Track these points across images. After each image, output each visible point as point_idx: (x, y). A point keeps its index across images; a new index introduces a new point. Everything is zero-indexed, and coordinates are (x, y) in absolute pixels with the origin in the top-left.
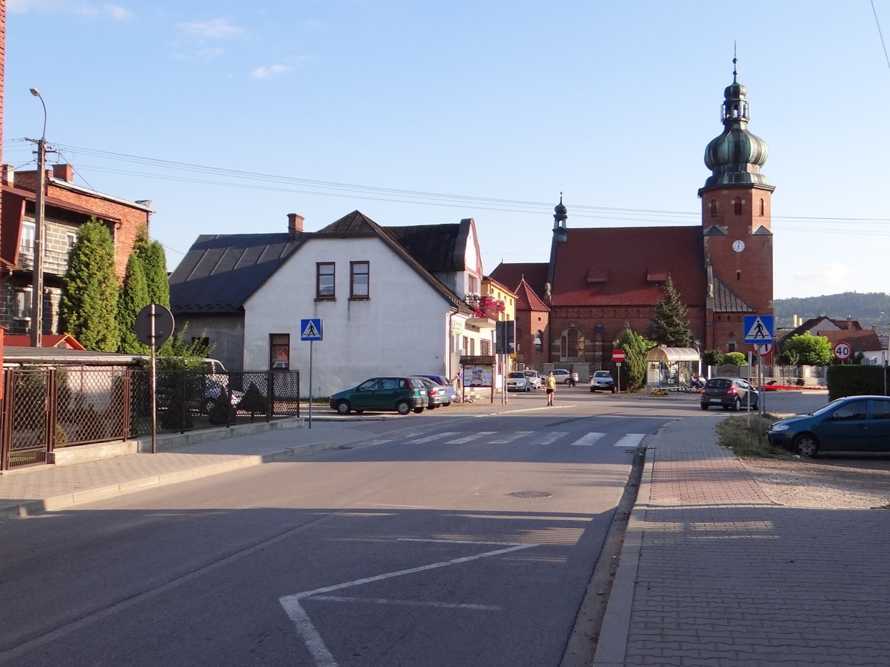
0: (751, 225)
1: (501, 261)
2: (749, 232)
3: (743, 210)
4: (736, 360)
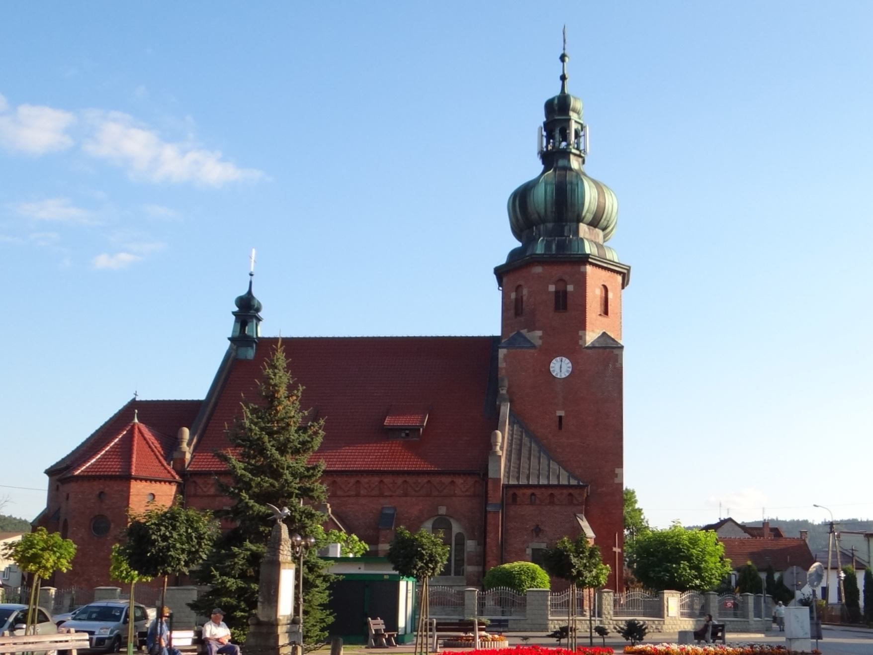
0: (584, 328)
1: (134, 396)
2: (581, 342)
3: (569, 302)
4: (520, 579)
